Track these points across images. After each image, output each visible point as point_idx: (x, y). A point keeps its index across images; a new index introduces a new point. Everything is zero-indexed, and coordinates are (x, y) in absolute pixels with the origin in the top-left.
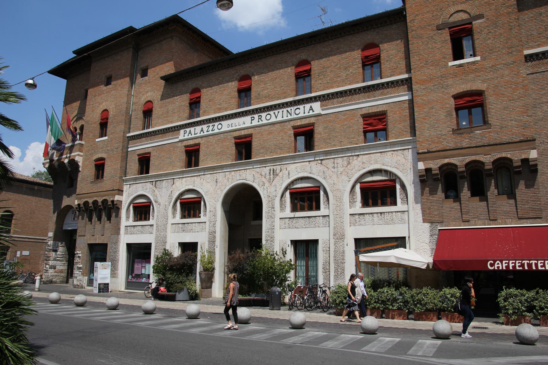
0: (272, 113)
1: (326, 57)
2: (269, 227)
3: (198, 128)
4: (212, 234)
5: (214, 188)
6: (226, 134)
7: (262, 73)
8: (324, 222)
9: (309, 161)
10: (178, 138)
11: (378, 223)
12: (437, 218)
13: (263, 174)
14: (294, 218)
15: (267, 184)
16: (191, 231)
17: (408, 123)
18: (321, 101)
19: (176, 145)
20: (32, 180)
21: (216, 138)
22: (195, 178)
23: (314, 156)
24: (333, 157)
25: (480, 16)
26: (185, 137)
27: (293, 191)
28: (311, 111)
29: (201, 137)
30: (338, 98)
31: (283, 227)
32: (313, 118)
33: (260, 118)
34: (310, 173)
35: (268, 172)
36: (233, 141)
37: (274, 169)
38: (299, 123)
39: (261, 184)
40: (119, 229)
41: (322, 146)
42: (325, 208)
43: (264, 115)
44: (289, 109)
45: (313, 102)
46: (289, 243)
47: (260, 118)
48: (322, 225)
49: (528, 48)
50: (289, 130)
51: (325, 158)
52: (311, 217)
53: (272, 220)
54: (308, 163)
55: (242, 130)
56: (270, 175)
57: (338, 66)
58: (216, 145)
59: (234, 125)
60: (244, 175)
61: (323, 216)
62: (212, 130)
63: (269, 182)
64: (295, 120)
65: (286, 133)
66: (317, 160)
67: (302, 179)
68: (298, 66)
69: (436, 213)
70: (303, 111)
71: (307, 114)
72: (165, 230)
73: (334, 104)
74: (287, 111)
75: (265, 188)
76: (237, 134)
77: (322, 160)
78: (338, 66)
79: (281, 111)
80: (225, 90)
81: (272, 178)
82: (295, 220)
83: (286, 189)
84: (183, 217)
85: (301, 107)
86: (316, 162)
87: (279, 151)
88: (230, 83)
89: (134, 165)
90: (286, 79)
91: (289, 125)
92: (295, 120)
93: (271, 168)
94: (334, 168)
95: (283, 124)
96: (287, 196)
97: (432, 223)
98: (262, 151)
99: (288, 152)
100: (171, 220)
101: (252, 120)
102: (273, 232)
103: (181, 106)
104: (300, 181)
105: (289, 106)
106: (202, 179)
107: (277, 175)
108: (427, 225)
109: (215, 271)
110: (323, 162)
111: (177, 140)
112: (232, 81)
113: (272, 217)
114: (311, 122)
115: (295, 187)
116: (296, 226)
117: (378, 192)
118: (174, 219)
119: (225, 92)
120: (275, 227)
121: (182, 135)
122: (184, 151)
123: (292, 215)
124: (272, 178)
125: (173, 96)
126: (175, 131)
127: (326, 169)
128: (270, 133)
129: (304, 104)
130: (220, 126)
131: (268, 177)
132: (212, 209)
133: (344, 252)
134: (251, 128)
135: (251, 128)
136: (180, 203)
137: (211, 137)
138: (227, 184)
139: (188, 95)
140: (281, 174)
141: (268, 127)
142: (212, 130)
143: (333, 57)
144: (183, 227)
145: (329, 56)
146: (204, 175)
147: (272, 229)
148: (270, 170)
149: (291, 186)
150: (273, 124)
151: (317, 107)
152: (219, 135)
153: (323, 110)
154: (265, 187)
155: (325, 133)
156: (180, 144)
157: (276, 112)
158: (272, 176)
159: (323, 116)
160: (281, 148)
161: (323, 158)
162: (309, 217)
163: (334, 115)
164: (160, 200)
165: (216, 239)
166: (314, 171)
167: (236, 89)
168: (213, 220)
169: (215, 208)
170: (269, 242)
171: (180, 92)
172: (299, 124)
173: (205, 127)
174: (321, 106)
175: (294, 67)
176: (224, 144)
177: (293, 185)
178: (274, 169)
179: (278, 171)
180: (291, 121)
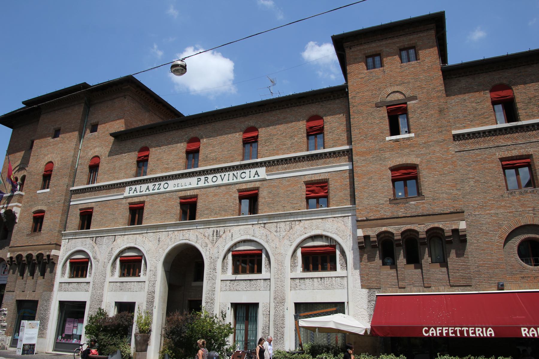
0: (218, 175)
1: (273, 125)
3: (144, 186)
4: (151, 294)
6: (171, 194)
8: (265, 286)
9: (253, 224)
11: (318, 288)
12: (374, 285)
13: (207, 235)
14: (235, 280)
15: (210, 246)
16: (129, 290)
17: (348, 191)
24: (276, 221)
25: (414, 98)
28: (256, 176)
29: (147, 195)
30: (283, 164)
31: (223, 289)
32: (258, 183)
33: (206, 180)
34: (253, 236)
35: (211, 234)
36: (178, 201)
37: (217, 231)
38: (244, 187)
39: (204, 245)
40: (53, 285)
41: (265, 210)
42: (266, 271)
43: (210, 177)
44: (235, 173)
46: (230, 306)
47: (206, 180)
48: (263, 288)
49: (455, 129)
50: (234, 193)
60: (187, 235)
62: (158, 189)
63: (212, 243)
66: (261, 224)
69: (374, 279)
70: (249, 175)
71: (252, 178)
72: (102, 288)
73: (278, 170)
74: (233, 174)
75: (208, 249)
76: (182, 194)
77: (265, 224)
78: (284, 135)
79: (227, 174)
81: (215, 240)
82: (236, 283)
83: (229, 251)
84: (122, 275)
85: (247, 171)
86: (259, 226)
87: (223, 213)
88: (179, 144)
89: (75, 219)
93: (215, 229)
94: (276, 232)
95: (228, 187)
97: (370, 288)
98: (206, 212)
99: (233, 215)
100: (109, 278)
102: (214, 294)
104: (242, 244)
107: (220, 237)
108: (365, 291)
109: (152, 333)
110: (267, 225)
112: (181, 142)
114: (256, 186)
115: (238, 249)
116: (237, 289)
117: (319, 258)
119: (174, 153)
120: (216, 289)
121: (127, 192)
123: (233, 277)
124: (215, 240)
127: (268, 233)
128: (215, 195)
130: (166, 186)
131: (211, 238)
132: (153, 269)
133: (283, 317)
134: (197, 189)
135: (197, 189)
137: (156, 196)
138: (170, 243)
140: (224, 236)
143: (279, 126)
145: (276, 124)
146: (147, 233)
147: (213, 290)
149: (234, 247)
151: (262, 172)
152: (164, 194)
153: (268, 175)
154: (208, 248)
155: (269, 197)
157: (223, 174)
158: (215, 237)
160: (225, 211)
161: (266, 222)
162: (250, 280)
164: (99, 257)
165: (155, 299)
166: (257, 234)
167: (185, 150)
168: (153, 280)
169: (156, 267)
170: (209, 304)
173: (151, 185)
176: (169, 203)
177: (236, 247)
178: (217, 231)
179: (221, 233)
180: (237, 184)
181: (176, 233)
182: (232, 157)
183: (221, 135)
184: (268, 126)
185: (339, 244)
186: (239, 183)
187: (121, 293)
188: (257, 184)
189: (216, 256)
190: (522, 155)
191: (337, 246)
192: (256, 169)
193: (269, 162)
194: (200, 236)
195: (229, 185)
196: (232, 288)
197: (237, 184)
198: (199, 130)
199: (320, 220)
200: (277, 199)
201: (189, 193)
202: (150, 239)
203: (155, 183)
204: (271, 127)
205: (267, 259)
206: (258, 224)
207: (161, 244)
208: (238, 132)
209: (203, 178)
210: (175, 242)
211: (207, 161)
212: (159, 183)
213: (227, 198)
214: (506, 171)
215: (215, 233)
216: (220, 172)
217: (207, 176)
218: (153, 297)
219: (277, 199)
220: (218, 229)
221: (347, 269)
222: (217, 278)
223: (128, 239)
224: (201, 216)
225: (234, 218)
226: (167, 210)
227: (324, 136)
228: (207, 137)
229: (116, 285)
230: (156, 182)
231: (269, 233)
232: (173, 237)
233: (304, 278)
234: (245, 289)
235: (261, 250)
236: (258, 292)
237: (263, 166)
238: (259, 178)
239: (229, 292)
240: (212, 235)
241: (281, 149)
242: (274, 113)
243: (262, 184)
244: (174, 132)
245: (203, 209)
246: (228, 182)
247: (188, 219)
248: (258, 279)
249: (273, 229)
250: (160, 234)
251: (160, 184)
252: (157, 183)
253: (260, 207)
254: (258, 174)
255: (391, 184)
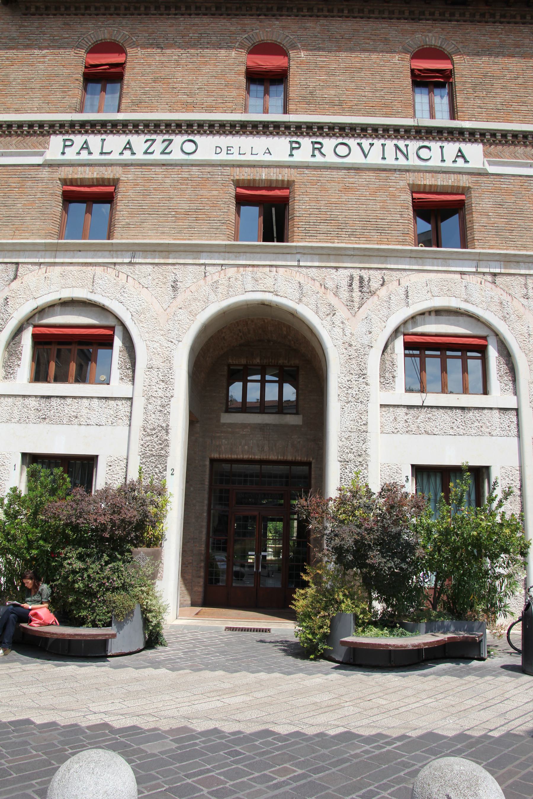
0: (352, 142)
1: (490, 55)
2: (351, 425)
4: (158, 434)
5: (165, 311)
6: (209, 169)
7: (319, 49)
8: (505, 425)
9: (462, 273)
10: (41, 154)
13: (330, 284)
14: (422, 407)
15: (342, 313)
16: (74, 419)
18: (484, 144)
19: (33, 173)
20: (230, 395)
21: (175, 174)
22: (99, 270)
23: (474, 263)
24: (523, 272)
26: (67, 157)
27: (410, 339)
28: (460, 161)
29: (125, 165)
30: (526, 146)
31: (388, 429)
32: (465, 177)
33: (318, 148)
34: (466, 301)
35: (344, 283)
36: (232, 191)
37: (361, 279)
38: (428, 180)
39: (324, 309)
41: (492, 243)
42: (503, 390)
44: (401, 144)
45: (464, 140)
46: (409, 472)
47: (318, 148)
48: (498, 431)
50: (401, 190)
51: (503, 271)
52: (469, 409)
53: (360, 406)
54: (458, 276)
55: (262, 167)
56: (352, 291)
57: (520, 81)
58: (173, 192)
59: (235, 150)
60: (269, 282)
61: (500, 409)
62: (163, 153)
64: (419, 171)
65: (393, 196)
66: (484, 274)
67: (439, 312)
68: (418, 55)
70: (440, 155)
71: (449, 163)
73: (516, 157)
74: (397, 147)
75: (338, 323)
76: (246, 174)
77: (495, 275)
78: (520, 81)
79: (378, 143)
80: (205, 63)
81: (357, 299)
82: (423, 414)
83: (396, 332)
84: (39, 375)
85: (435, 145)
86: (478, 279)
87: (375, 236)
88: (223, 51)
90: (388, 76)
91: (403, 182)
92: (419, 171)
93: (356, 274)
95: (383, 175)
96: (396, 351)
98: (323, 228)
99: (403, 243)
101: (293, 149)
102: (364, 441)
103: (57, 76)
104: (433, 317)
105: (402, 137)
106: (123, 277)
107: (372, 293)
109: (165, 544)
110: (499, 280)
111: (38, 160)
112: (229, 48)
113: (359, 400)
114: (461, 184)
115: (420, 329)
116: (428, 429)
118: (7, 383)
119: (205, 69)
120: (370, 428)
121: (55, 147)
122: (60, 193)
123: (416, 399)
124: (357, 299)
125: (28, 47)
126: (29, 134)
127: (505, 297)
128: (347, 189)
129: (440, 139)
130: (189, 147)
131: (344, 294)
132: (157, 362)
134: (289, 167)
135: (289, 167)
136: (35, 336)
137: (158, 169)
138: (212, 297)
139: (83, 53)
141: (343, 173)
142: (163, 153)
143: (506, 60)
144: (45, 411)
145: (497, 55)
146: (130, 263)
147: (362, 430)
148: (352, 278)
149: (409, 325)
150: (357, 169)
151: (475, 153)
152: (185, 169)
153: (490, 163)
154: (337, 319)
155: (499, 216)
156: (45, 173)
157: (366, 143)
158: (356, 294)
159: (492, 178)
160: (380, 230)
161: (497, 271)
162: (463, 408)
163: (517, 181)
165: (171, 449)
166: (476, 296)
167: (243, 69)
168: (160, 393)
169: (168, 360)
170: (351, 465)
171: (53, 41)
172: (428, 182)
173: (139, 141)
174: (485, 155)
175: (408, 56)
176: (204, 192)
177: (415, 325)
178: (361, 279)
179: (375, 285)
180: (408, 171)
181: (231, 271)
182: (386, 106)
183: (351, 50)
184: (477, 54)
185: (497, 334)
186: (414, 171)
187: (43, 427)
188: (464, 181)
189: (366, 341)
190: (103, 179)
191: (118, 331)
192: (84, 137)
193: (493, 133)
194: (308, 286)
195: (384, 170)
196: (413, 428)
197: (408, 171)
198: (284, 27)
199: (150, 268)
200: (520, 223)
201: (264, 175)
202: (142, 281)
203: (154, 137)
204: (485, 59)
205: (502, 361)
206: (477, 273)
207: (181, 297)
208: (399, 53)
209: (306, 142)
210: (228, 296)
211: (311, 102)
212: (166, 137)
213: (384, 201)
214: (242, 208)
215: (356, 284)
216: (359, 136)
217: (72, 137)
218: (165, 444)
219: (520, 223)
220: (365, 274)
221: (133, 384)
222: (371, 399)
223: (62, 275)
224: (308, 235)
225: (312, 248)
226: (196, 211)
227: (122, 88)
228: (306, 47)
229: (25, 406)
230: (155, 132)
231: (509, 298)
232: (224, 281)
233: (49, 397)
234: (451, 432)
235: (112, 328)
236: (487, 439)
237: (476, 141)
238: (467, 165)
239: (407, 436)
240: (346, 288)
241: (518, 112)
242: (489, 28)
243: (477, 182)
244: (206, 20)
245: (312, 219)
246: (380, 161)
247: (262, 240)
248: (483, 408)
249: (518, 290)
250: (179, 271)
251: (171, 141)
252: (159, 138)
253: (477, 236)
254: (130, 148)
255: (233, 208)
